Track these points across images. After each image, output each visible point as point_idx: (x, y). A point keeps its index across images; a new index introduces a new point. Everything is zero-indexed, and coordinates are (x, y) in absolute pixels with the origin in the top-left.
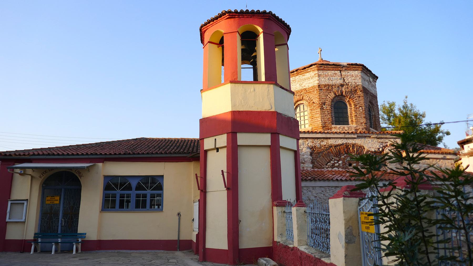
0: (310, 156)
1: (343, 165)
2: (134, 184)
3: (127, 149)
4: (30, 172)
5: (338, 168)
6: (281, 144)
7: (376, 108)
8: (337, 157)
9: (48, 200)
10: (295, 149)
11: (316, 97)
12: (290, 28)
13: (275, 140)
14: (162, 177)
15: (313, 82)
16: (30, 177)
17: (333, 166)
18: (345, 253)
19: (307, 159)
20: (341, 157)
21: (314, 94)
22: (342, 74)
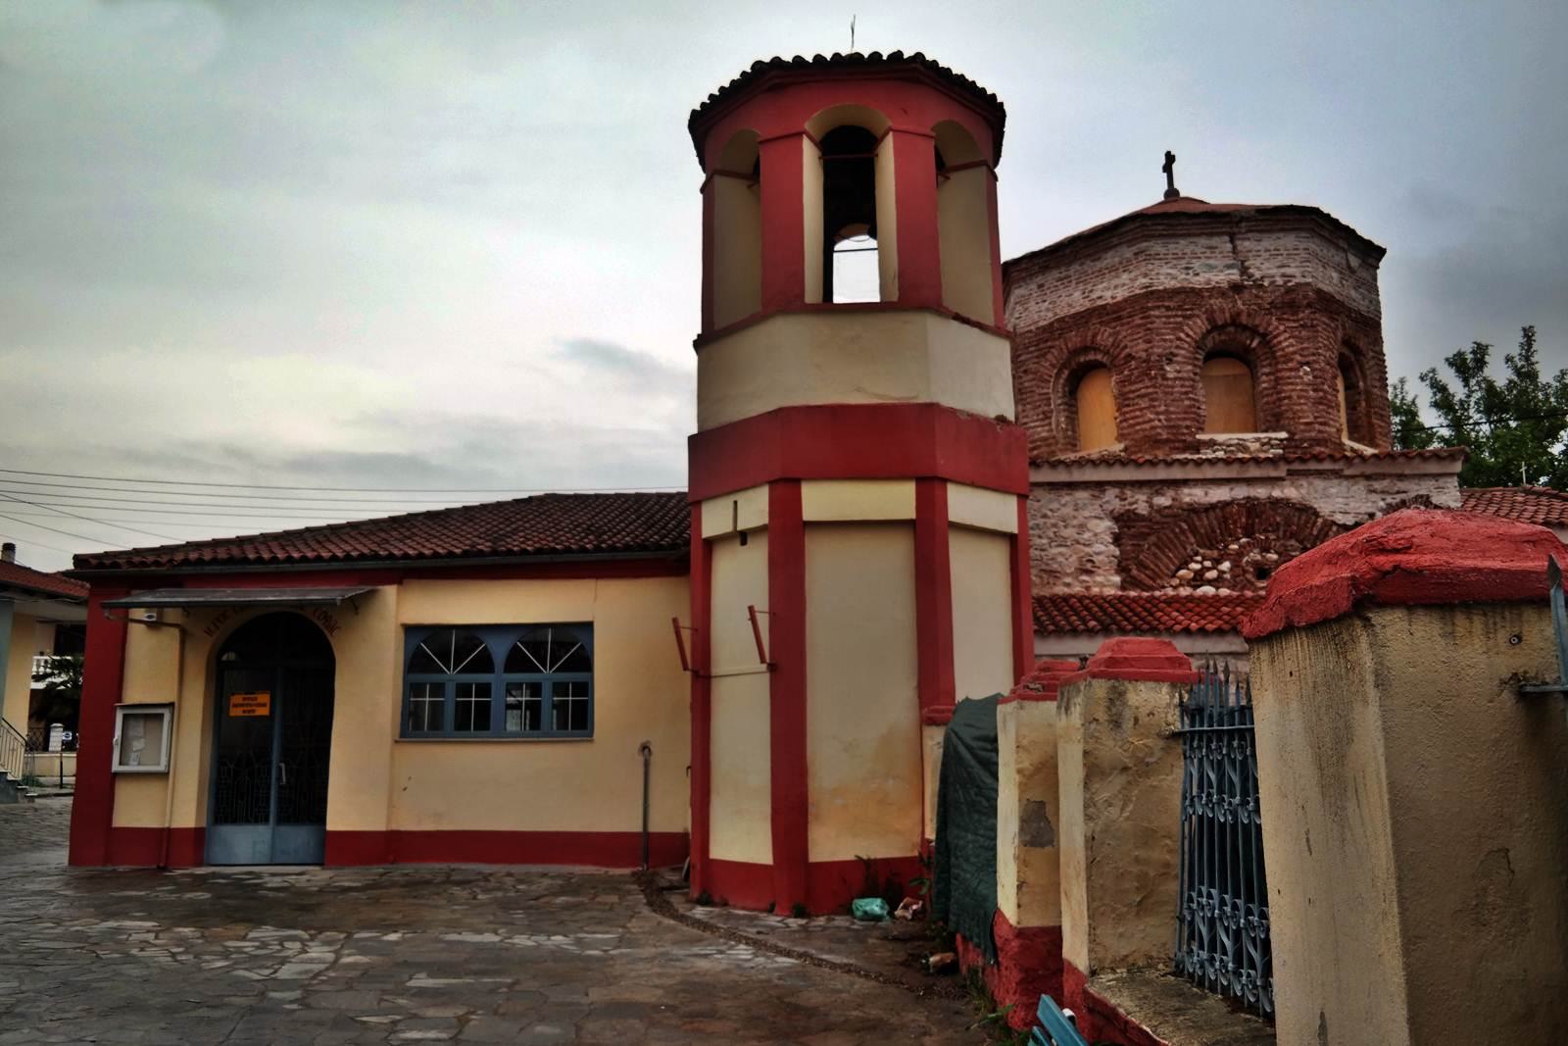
0: (1112, 547)
1: (1234, 577)
2: (499, 650)
3: (567, 529)
4: (172, 615)
5: (1217, 588)
6: (954, 515)
7: (1372, 363)
8: (1211, 547)
9: (235, 706)
10: (1013, 527)
11: (1139, 335)
12: (1002, 104)
13: (786, 506)
14: (588, 626)
15: (1127, 282)
16: (176, 632)
17: (1198, 579)
18: (1019, 876)
19: (1101, 558)
20: (1226, 547)
21: (1132, 325)
22: (1239, 248)
